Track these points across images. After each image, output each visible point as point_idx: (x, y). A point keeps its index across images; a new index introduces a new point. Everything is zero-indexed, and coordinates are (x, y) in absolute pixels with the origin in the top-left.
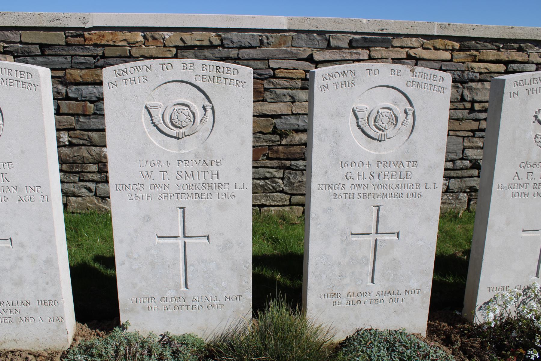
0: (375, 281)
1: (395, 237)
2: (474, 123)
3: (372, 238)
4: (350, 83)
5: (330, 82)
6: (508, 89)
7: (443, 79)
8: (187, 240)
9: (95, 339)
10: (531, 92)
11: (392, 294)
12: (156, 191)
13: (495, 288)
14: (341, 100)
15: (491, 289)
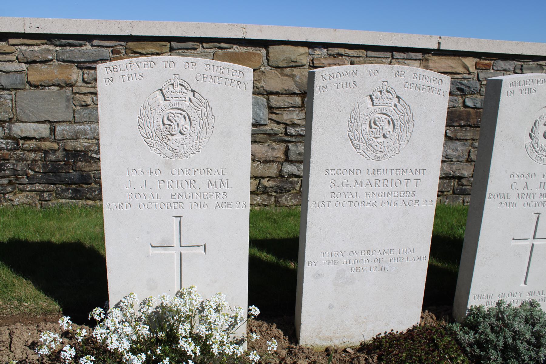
0: (527, 283)
2: (472, 123)
4: (532, 90)
5: (517, 89)
6: (505, 89)
8: (184, 251)
10: (523, 92)
13: (480, 296)
14: (340, 97)
15: (476, 297)
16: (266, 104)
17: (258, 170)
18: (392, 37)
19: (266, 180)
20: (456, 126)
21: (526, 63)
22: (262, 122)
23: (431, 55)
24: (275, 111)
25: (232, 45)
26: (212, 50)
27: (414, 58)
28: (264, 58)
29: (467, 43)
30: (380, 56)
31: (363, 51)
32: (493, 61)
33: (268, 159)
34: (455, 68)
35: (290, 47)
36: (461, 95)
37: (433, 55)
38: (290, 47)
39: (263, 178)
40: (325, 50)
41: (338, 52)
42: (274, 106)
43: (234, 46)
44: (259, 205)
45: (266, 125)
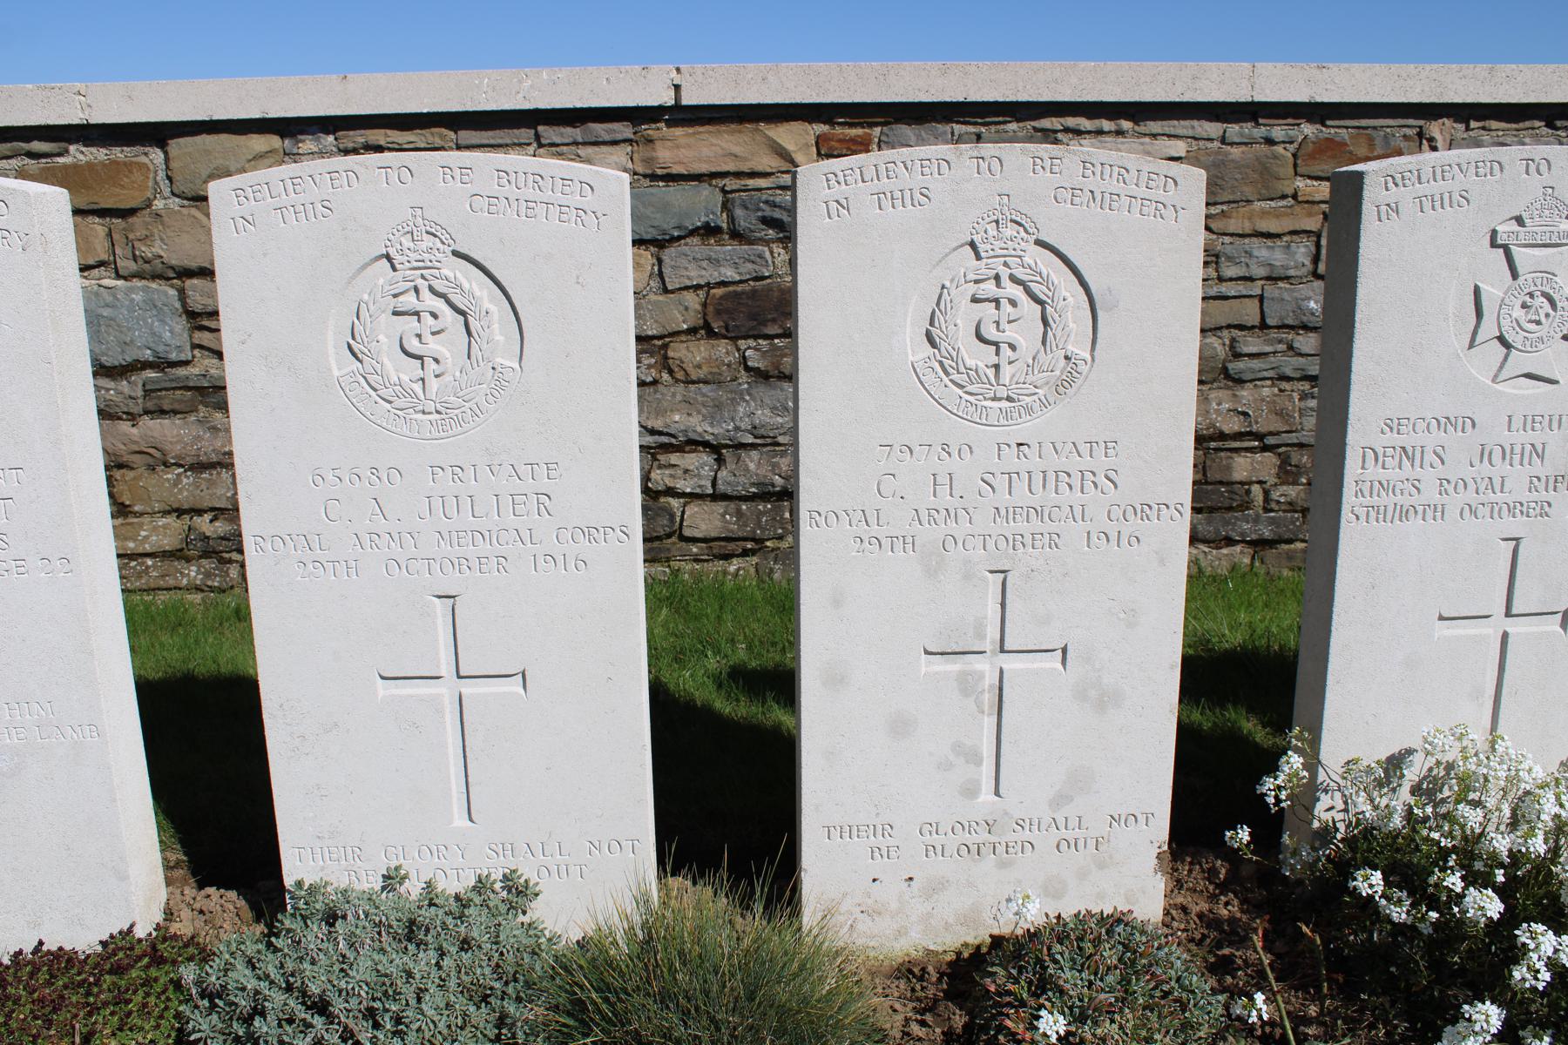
1: (514, 686)
2: (725, 324)
3: (1490, 631)
5: (1404, 196)
6: (1373, 195)
7: (1176, 183)
8: (468, 688)
9: (702, 904)
10: (1427, 205)
11: (1062, 826)
12: (1455, 501)
14: (871, 253)
16: (178, 305)
17: (180, 491)
18: (520, 82)
19: (208, 517)
20: (778, 336)
21: (993, 128)
22: (173, 356)
23: (662, 125)
24: (206, 323)
25: (63, 144)
26: (13, 162)
27: (607, 138)
28: (161, 175)
29: (770, 77)
30: (500, 141)
31: (444, 131)
32: (878, 130)
33: (203, 459)
34: (745, 159)
35: (224, 137)
36: (780, 240)
37: (670, 124)
38: (224, 138)
39: (200, 512)
40: (331, 138)
41: (853, 124)
42: (198, 308)
43: (72, 148)
44: (198, 589)
45: (186, 363)
